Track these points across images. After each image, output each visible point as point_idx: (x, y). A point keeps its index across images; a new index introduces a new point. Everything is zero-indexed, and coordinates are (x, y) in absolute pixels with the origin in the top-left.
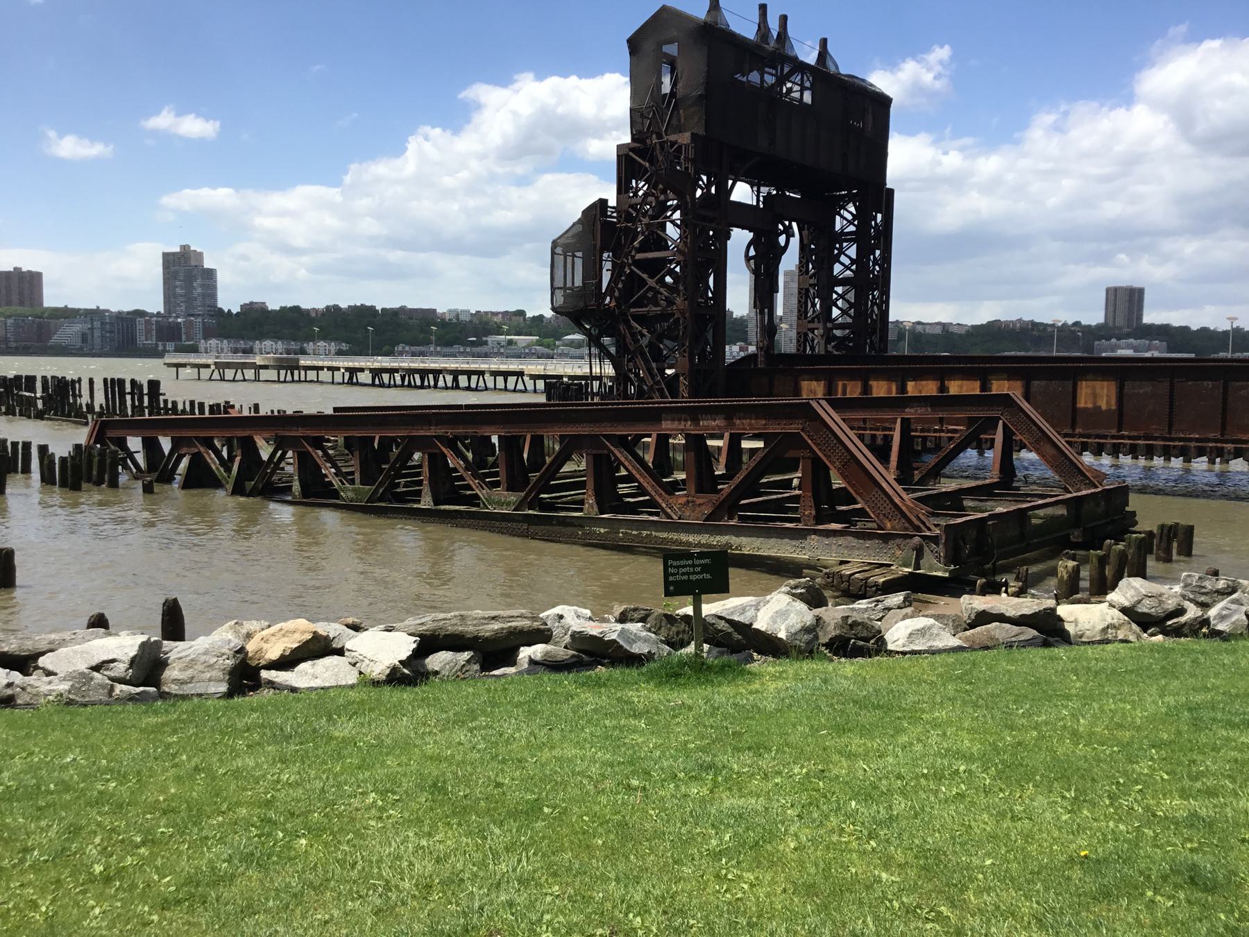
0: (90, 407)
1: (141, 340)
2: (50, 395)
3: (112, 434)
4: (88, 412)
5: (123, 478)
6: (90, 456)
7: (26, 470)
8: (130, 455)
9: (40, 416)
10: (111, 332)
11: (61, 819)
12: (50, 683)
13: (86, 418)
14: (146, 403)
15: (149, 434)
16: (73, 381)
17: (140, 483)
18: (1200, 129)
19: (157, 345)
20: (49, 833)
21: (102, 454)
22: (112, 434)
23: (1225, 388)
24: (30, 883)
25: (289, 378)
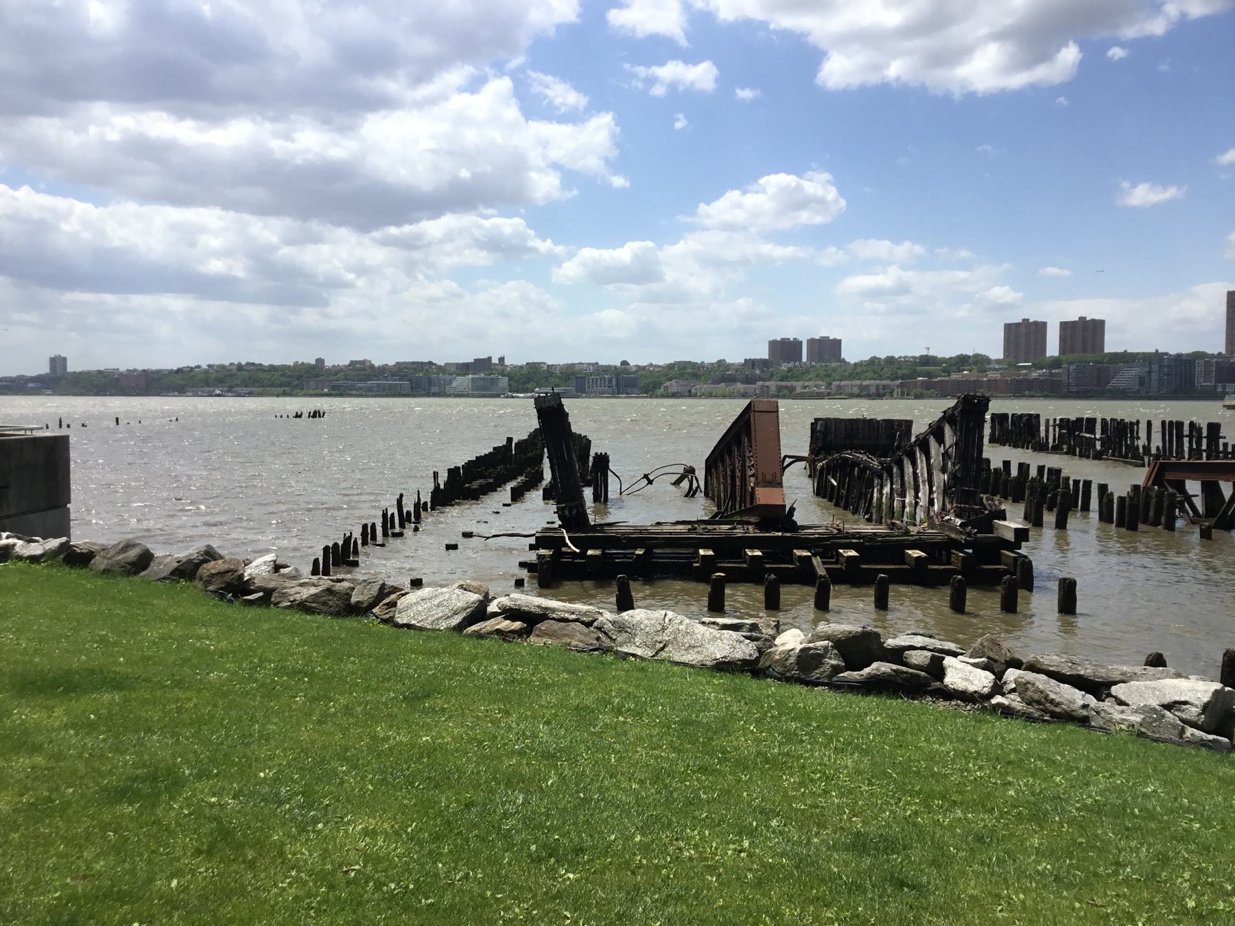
0: (1147, 449)
1: (1200, 382)
2: (1109, 438)
3: (1170, 476)
4: (1145, 454)
5: (1179, 524)
6: (1148, 497)
7: (1086, 508)
8: (1188, 498)
9: (1098, 456)
10: (1168, 374)
11: (1150, 845)
12: (1122, 712)
13: (1142, 459)
14: (1204, 447)
15: (1209, 478)
16: (1132, 424)
17: (1198, 530)
18: (509, 502)
19: (1215, 387)
20: (1138, 854)
21: (1160, 496)
22: (1170, 476)
24: (1125, 896)
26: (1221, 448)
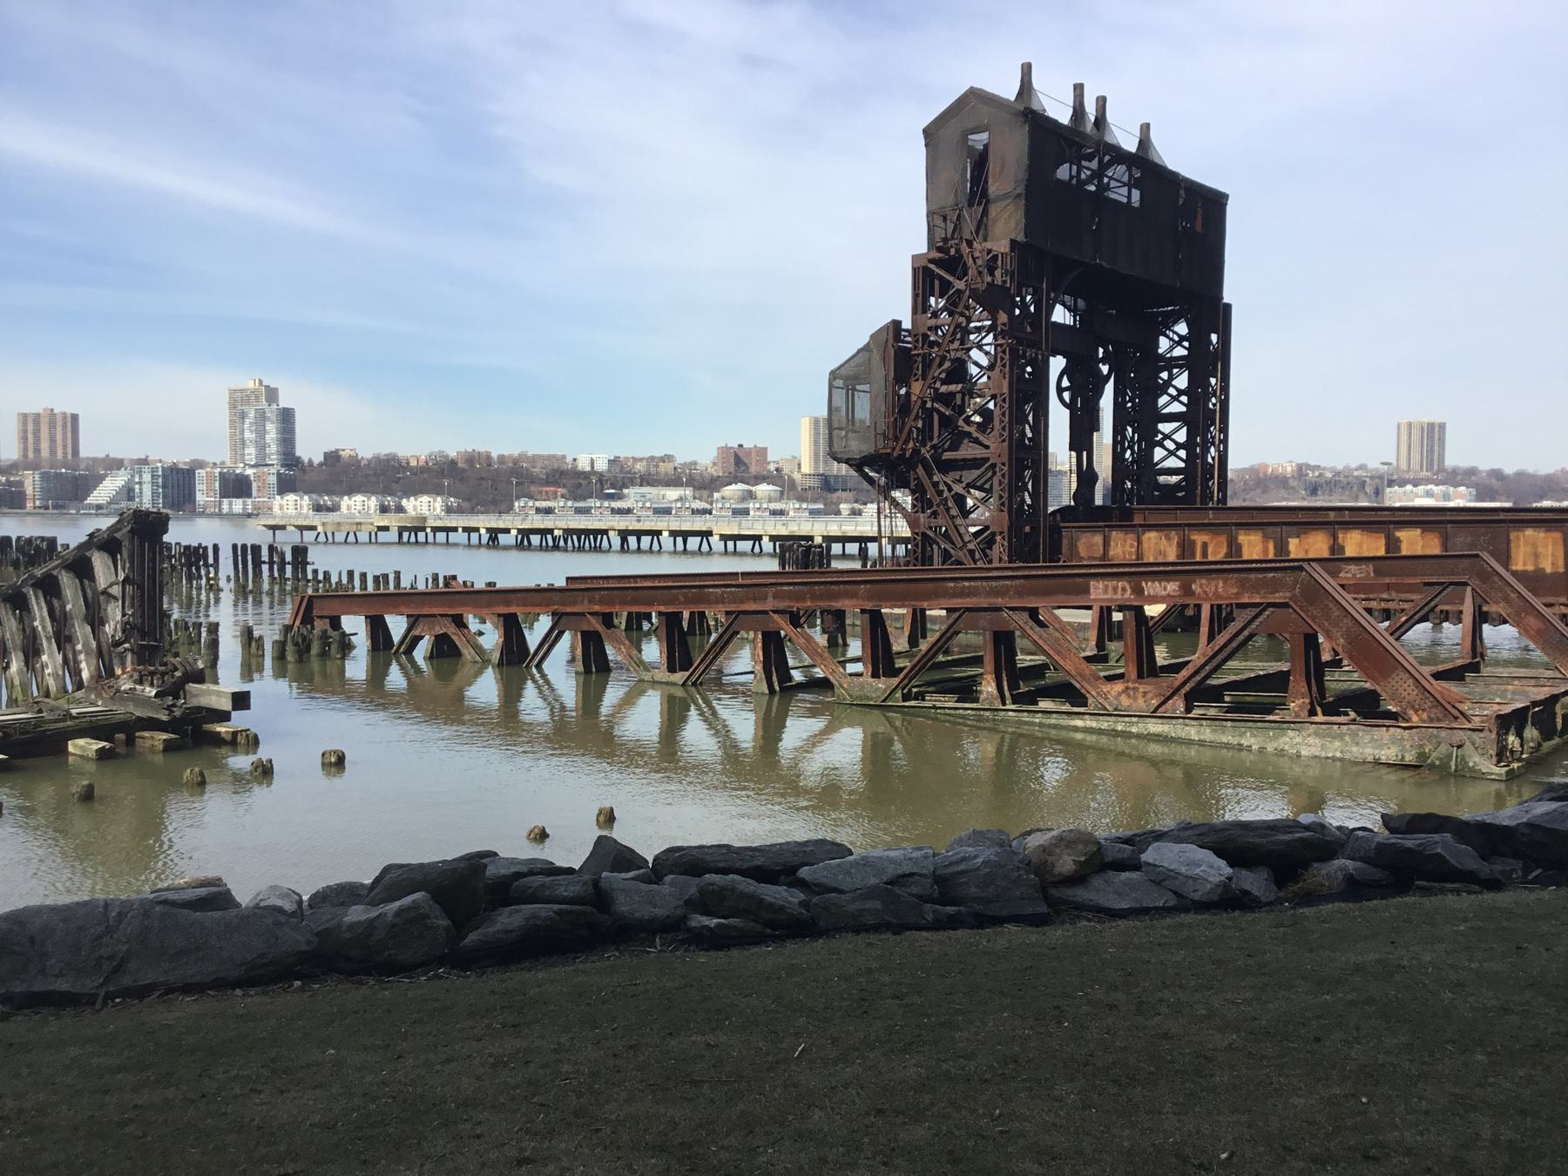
23: (1139, 542)
25: (413, 539)
26: (310, 576)
